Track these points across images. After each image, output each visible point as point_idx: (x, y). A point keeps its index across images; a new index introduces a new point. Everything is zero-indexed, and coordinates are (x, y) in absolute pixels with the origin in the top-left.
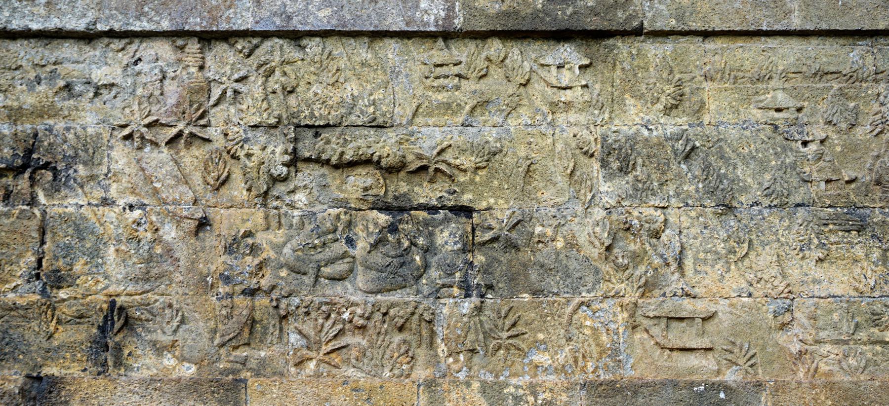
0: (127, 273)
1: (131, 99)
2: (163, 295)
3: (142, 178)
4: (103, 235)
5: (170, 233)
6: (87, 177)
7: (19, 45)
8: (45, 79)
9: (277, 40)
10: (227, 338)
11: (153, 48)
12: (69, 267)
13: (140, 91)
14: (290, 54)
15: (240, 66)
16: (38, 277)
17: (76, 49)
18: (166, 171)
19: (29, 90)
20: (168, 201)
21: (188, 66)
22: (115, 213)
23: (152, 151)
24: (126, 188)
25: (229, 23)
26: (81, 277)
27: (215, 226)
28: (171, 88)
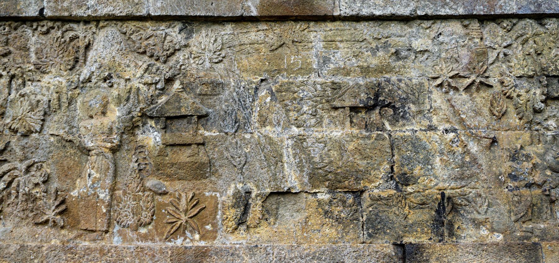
0: (450, 175)
1: (438, 60)
2: (473, 188)
3: (452, 112)
4: (431, 149)
5: (474, 147)
6: (417, 112)
7: (363, 25)
8: (381, 47)
9: (528, 20)
10: (519, 216)
11: (450, 26)
12: (411, 172)
13: (443, 55)
14: (537, 29)
15: (506, 37)
16: (392, 178)
17: (399, 27)
18: (468, 107)
19: (373, 55)
20: (471, 127)
21: (474, 38)
22: (438, 135)
23: (454, 94)
24: (442, 118)
25: (501, 9)
26: (421, 178)
27: (500, 142)
28: (463, 52)
